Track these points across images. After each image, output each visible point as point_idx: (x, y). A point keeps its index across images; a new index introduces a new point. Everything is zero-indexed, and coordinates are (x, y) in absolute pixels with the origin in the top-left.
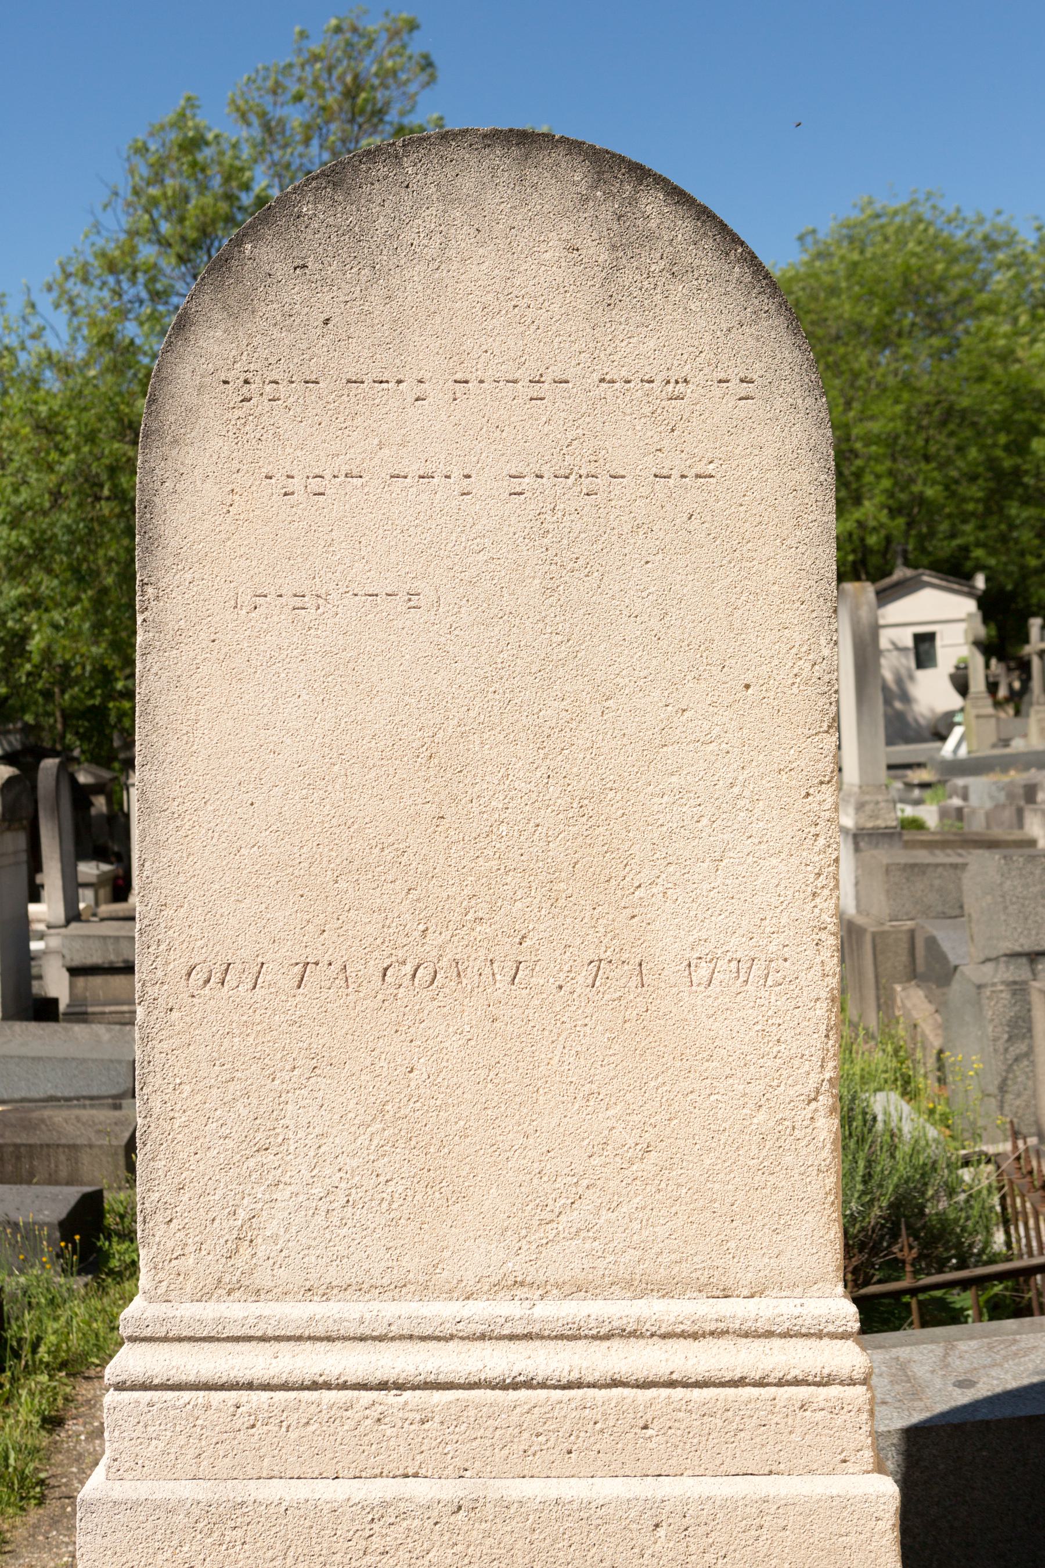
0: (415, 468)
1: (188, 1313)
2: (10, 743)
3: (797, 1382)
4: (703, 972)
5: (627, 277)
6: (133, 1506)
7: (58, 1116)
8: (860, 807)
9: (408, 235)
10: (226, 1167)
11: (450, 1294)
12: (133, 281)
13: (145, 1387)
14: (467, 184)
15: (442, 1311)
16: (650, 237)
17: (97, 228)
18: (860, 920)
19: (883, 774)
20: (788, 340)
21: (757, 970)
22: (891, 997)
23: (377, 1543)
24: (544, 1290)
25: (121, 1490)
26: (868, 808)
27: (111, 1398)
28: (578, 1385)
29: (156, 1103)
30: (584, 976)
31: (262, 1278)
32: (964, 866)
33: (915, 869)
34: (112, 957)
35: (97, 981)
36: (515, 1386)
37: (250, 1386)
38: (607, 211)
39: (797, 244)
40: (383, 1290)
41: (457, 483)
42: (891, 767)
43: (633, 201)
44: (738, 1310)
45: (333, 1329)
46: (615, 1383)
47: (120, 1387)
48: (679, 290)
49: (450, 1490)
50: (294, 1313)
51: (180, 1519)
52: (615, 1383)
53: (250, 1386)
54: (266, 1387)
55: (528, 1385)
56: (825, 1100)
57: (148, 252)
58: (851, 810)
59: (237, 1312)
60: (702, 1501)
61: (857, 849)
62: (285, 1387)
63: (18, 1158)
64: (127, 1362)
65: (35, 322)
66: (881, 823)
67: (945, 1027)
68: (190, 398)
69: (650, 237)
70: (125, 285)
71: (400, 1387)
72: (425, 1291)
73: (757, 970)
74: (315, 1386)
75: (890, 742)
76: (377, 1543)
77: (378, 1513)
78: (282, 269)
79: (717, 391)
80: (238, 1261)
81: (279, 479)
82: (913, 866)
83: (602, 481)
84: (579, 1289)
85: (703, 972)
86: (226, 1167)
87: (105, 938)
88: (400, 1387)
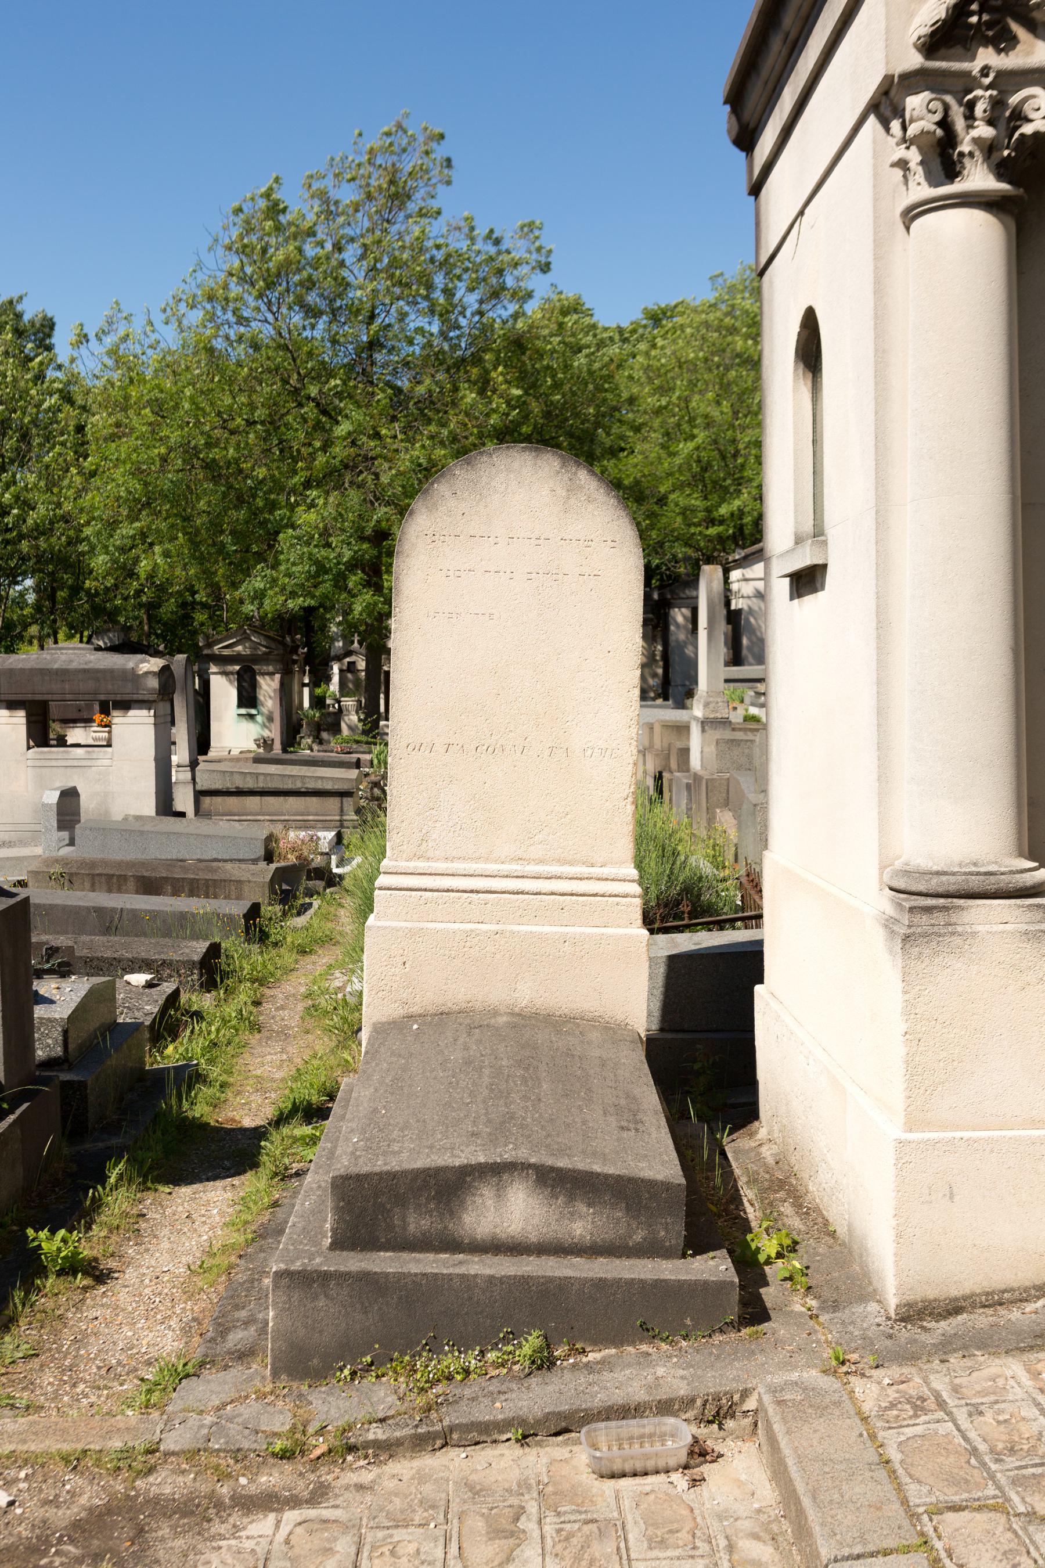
0: (493, 569)
1: (404, 865)
2: (110, 639)
3: (616, 896)
4: (589, 752)
5: (572, 501)
6: (385, 928)
7: (228, 866)
8: (706, 705)
9: (493, 484)
10: (418, 815)
11: (496, 862)
12: (224, 310)
13: (389, 889)
14: (516, 465)
15: (492, 867)
16: (581, 487)
17: (200, 266)
18: (701, 773)
19: (722, 685)
20: (629, 527)
21: (609, 752)
22: (714, 814)
23: (468, 944)
24: (529, 861)
25: (379, 924)
26: (711, 706)
27: (377, 892)
28: (539, 894)
29: (395, 792)
30: (547, 752)
31: (430, 854)
32: (752, 741)
33: (733, 742)
34: (229, 785)
35: (219, 800)
36: (518, 893)
37: (425, 890)
38: (566, 478)
39: (709, 283)
40: (472, 859)
41: (508, 575)
42: (727, 681)
43: (575, 474)
44: (596, 871)
45: (455, 872)
46: (553, 894)
47: (380, 889)
48: (591, 507)
49: (494, 927)
50: (441, 866)
51: (401, 933)
52: (553, 894)
53: (425, 890)
54: (431, 890)
55: (522, 893)
56: (630, 799)
57: (235, 290)
58: (701, 707)
59: (421, 865)
60: (581, 934)
61: (703, 731)
62: (438, 891)
63: (207, 887)
64: (382, 880)
65: (153, 337)
66: (719, 715)
67: (739, 828)
68: (413, 539)
69: (581, 487)
70: (219, 313)
71: (478, 892)
72: (487, 860)
73: (609, 752)
74: (448, 891)
75: (727, 664)
76: (468, 944)
77: (468, 934)
78: (448, 494)
79: (603, 544)
80: (422, 848)
81: (445, 571)
82: (732, 741)
83: (560, 576)
84: (541, 862)
85: (589, 752)
86: (418, 815)
87: (224, 772)
88: (478, 892)
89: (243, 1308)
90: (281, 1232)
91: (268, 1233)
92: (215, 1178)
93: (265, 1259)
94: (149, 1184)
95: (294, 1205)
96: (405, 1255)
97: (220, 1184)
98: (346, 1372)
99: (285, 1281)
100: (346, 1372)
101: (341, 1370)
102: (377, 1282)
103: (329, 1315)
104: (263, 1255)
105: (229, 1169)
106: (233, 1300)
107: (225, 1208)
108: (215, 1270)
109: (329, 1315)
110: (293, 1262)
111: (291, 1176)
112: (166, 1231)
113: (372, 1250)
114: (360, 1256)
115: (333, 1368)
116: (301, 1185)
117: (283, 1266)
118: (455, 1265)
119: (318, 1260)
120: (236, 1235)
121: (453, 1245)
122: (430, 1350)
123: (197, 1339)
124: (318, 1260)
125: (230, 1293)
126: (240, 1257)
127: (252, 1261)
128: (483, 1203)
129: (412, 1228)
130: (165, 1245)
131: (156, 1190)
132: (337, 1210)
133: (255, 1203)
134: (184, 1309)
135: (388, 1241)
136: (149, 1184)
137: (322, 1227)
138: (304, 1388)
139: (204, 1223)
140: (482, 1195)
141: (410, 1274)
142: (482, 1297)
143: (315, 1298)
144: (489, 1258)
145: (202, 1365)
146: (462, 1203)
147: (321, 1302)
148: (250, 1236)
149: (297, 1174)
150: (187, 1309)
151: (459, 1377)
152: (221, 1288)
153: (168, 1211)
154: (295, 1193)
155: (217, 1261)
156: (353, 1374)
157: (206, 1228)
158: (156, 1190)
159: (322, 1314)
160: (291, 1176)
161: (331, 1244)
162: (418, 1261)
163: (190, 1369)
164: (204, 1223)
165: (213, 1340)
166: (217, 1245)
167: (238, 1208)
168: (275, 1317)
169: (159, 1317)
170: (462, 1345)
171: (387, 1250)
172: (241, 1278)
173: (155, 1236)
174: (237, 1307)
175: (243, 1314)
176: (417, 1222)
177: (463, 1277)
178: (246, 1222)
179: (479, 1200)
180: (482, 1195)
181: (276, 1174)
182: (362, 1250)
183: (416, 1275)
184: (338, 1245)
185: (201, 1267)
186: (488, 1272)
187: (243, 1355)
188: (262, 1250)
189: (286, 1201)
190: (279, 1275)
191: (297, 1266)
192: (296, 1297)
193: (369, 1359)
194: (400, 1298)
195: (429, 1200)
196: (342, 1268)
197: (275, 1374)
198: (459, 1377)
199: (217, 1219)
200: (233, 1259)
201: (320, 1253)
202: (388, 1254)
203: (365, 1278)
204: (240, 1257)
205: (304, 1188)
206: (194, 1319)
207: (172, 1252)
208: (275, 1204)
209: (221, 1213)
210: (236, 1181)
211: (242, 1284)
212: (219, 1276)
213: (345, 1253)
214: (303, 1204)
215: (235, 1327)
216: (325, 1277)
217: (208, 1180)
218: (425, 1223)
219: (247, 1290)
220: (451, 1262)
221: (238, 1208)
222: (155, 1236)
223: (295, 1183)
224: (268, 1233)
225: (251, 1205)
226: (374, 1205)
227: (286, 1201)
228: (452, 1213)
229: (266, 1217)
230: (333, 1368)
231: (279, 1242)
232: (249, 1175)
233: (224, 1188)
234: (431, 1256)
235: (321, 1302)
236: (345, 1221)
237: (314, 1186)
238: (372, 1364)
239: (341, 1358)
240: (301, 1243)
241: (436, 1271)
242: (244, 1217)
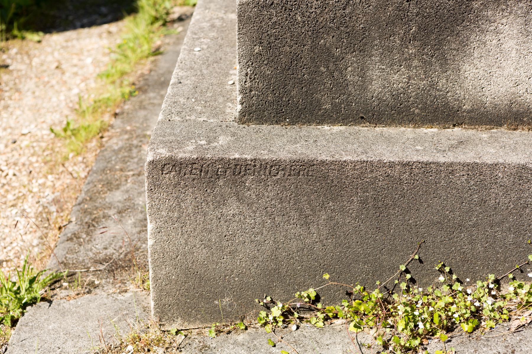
89: (118, 187)
90: (164, 84)
91: (148, 86)
92: (90, 25)
93: (146, 119)
94: (16, 32)
95: (178, 53)
96: (365, 131)
97: (95, 30)
98: (276, 311)
99: (170, 177)
100: (276, 311)
101: (268, 308)
102: (325, 177)
103: (245, 234)
104: (142, 113)
105: (105, 16)
106: (106, 178)
107: (99, 57)
108: (83, 133)
109: (245, 234)
110: (180, 144)
111: (173, 21)
112: (30, 84)
113: (309, 122)
114: (293, 131)
115: (254, 306)
116: (185, 31)
117: (164, 152)
118: (452, 147)
119: (223, 140)
120: (111, 88)
121: (444, 113)
122: (412, 281)
123: (53, 233)
124: (223, 140)
125: (102, 165)
126: (116, 115)
127: (129, 121)
128: (499, 45)
129: (375, 87)
130: (28, 100)
131: (23, 38)
132: (251, 60)
133: (134, 50)
134: (43, 185)
135: (336, 108)
136: (16, 32)
137: (222, 84)
138: (210, 333)
139: (76, 74)
140: (497, 32)
141: (381, 164)
142: (503, 200)
143: (222, 202)
144: (502, 133)
145: (55, 282)
146: (464, 44)
147: (232, 208)
148: (127, 90)
149: (180, 19)
150: (47, 188)
151: (466, 327)
152: (91, 157)
153: (36, 61)
154: (179, 40)
155: (88, 119)
156: (287, 314)
157: (78, 80)
158: (23, 38)
159: (234, 226)
160: (173, 21)
161: (243, 113)
162: (389, 140)
163: (39, 291)
164: (76, 74)
165: (74, 237)
166: (90, 99)
167: (114, 56)
168: (158, 231)
169: (10, 197)
170: (461, 273)
171: (333, 121)
172: (115, 143)
173: (18, 90)
174: (111, 186)
175: (117, 197)
176: (383, 77)
177: (473, 168)
178: (123, 74)
179: (491, 40)
180: (497, 32)
181: (156, 19)
182: (293, 123)
183: (392, 165)
184: (252, 114)
185: (65, 130)
186: (516, 159)
187: (118, 266)
188: (142, 107)
189: (169, 48)
190: (159, 167)
191: (187, 152)
192: (189, 205)
193: (312, 293)
194: (364, 202)
195: (405, 42)
196: (265, 155)
197: (164, 313)
198: (466, 327)
199: (91, 69)
200: (107, 118)
201: (223, 128)
202: (337, 128)
203: (304, 170)
204: (116, 115)
205: (189, 33)
206: (56, 201)
207: (36, 110)
208: (157, 52)
209: (96, 63)
210: (113, 27)
211: (116, 152)
212: (87, 140)
213: (265, 128)
214: (191, 51)
215: (106, 217)
216: (237, 171)
217: (83, 26)
218: (398, 79)
219: (124, 162)
220: (446, 144)
221: (114, 56)
222: (18, 90)
223: (178, 28)
224: (148, 86)
225: (129, 53)
226: (312, 50)
227: (169, 48)
228: (444, 61)
229: (146, 67)
230: (254, 306)
231: (162, 97)
232: (127, 22)
233: (100, 36)
234: (408, 132)
235: (232, 208)
236: (264, 76)
237: (206, 25)
238: (317, 299)
239: (267, 290)
240: (192, 110)
241: (425, 159)
242: (120, 67)
